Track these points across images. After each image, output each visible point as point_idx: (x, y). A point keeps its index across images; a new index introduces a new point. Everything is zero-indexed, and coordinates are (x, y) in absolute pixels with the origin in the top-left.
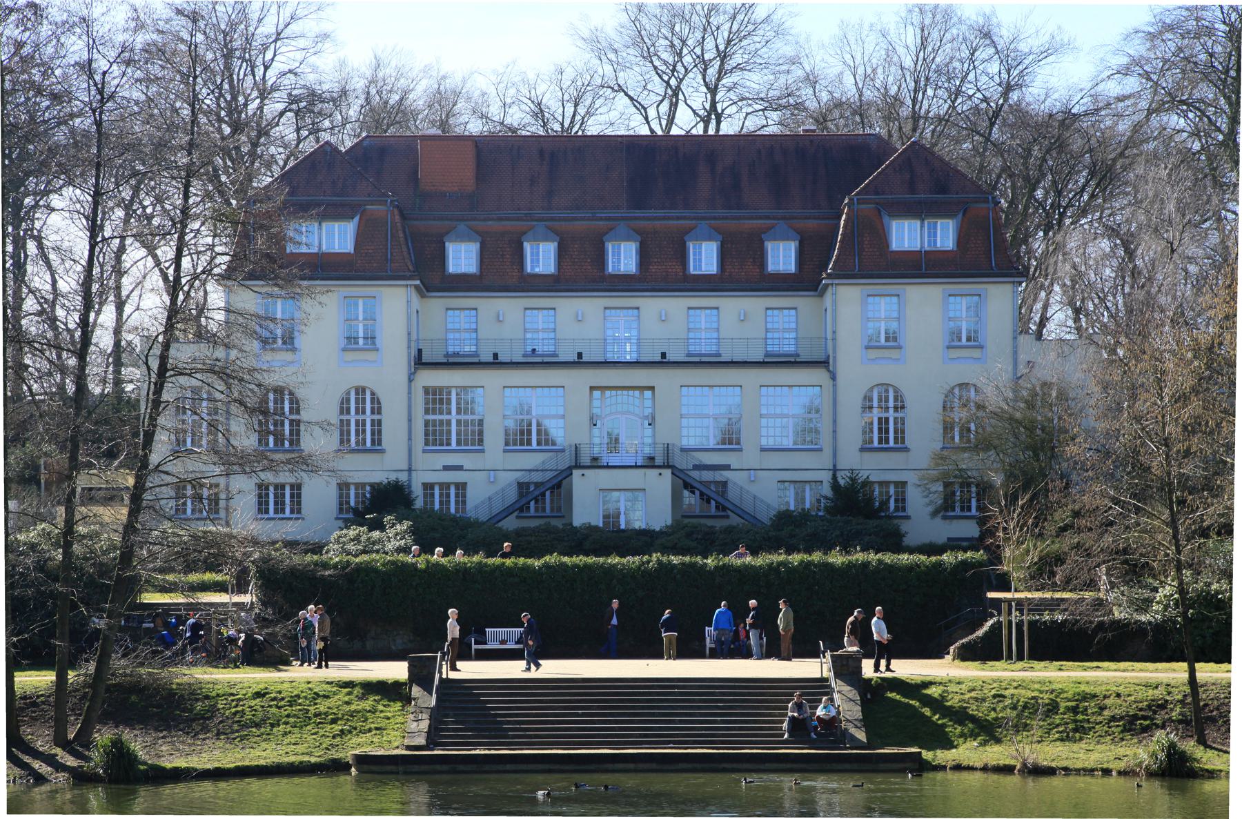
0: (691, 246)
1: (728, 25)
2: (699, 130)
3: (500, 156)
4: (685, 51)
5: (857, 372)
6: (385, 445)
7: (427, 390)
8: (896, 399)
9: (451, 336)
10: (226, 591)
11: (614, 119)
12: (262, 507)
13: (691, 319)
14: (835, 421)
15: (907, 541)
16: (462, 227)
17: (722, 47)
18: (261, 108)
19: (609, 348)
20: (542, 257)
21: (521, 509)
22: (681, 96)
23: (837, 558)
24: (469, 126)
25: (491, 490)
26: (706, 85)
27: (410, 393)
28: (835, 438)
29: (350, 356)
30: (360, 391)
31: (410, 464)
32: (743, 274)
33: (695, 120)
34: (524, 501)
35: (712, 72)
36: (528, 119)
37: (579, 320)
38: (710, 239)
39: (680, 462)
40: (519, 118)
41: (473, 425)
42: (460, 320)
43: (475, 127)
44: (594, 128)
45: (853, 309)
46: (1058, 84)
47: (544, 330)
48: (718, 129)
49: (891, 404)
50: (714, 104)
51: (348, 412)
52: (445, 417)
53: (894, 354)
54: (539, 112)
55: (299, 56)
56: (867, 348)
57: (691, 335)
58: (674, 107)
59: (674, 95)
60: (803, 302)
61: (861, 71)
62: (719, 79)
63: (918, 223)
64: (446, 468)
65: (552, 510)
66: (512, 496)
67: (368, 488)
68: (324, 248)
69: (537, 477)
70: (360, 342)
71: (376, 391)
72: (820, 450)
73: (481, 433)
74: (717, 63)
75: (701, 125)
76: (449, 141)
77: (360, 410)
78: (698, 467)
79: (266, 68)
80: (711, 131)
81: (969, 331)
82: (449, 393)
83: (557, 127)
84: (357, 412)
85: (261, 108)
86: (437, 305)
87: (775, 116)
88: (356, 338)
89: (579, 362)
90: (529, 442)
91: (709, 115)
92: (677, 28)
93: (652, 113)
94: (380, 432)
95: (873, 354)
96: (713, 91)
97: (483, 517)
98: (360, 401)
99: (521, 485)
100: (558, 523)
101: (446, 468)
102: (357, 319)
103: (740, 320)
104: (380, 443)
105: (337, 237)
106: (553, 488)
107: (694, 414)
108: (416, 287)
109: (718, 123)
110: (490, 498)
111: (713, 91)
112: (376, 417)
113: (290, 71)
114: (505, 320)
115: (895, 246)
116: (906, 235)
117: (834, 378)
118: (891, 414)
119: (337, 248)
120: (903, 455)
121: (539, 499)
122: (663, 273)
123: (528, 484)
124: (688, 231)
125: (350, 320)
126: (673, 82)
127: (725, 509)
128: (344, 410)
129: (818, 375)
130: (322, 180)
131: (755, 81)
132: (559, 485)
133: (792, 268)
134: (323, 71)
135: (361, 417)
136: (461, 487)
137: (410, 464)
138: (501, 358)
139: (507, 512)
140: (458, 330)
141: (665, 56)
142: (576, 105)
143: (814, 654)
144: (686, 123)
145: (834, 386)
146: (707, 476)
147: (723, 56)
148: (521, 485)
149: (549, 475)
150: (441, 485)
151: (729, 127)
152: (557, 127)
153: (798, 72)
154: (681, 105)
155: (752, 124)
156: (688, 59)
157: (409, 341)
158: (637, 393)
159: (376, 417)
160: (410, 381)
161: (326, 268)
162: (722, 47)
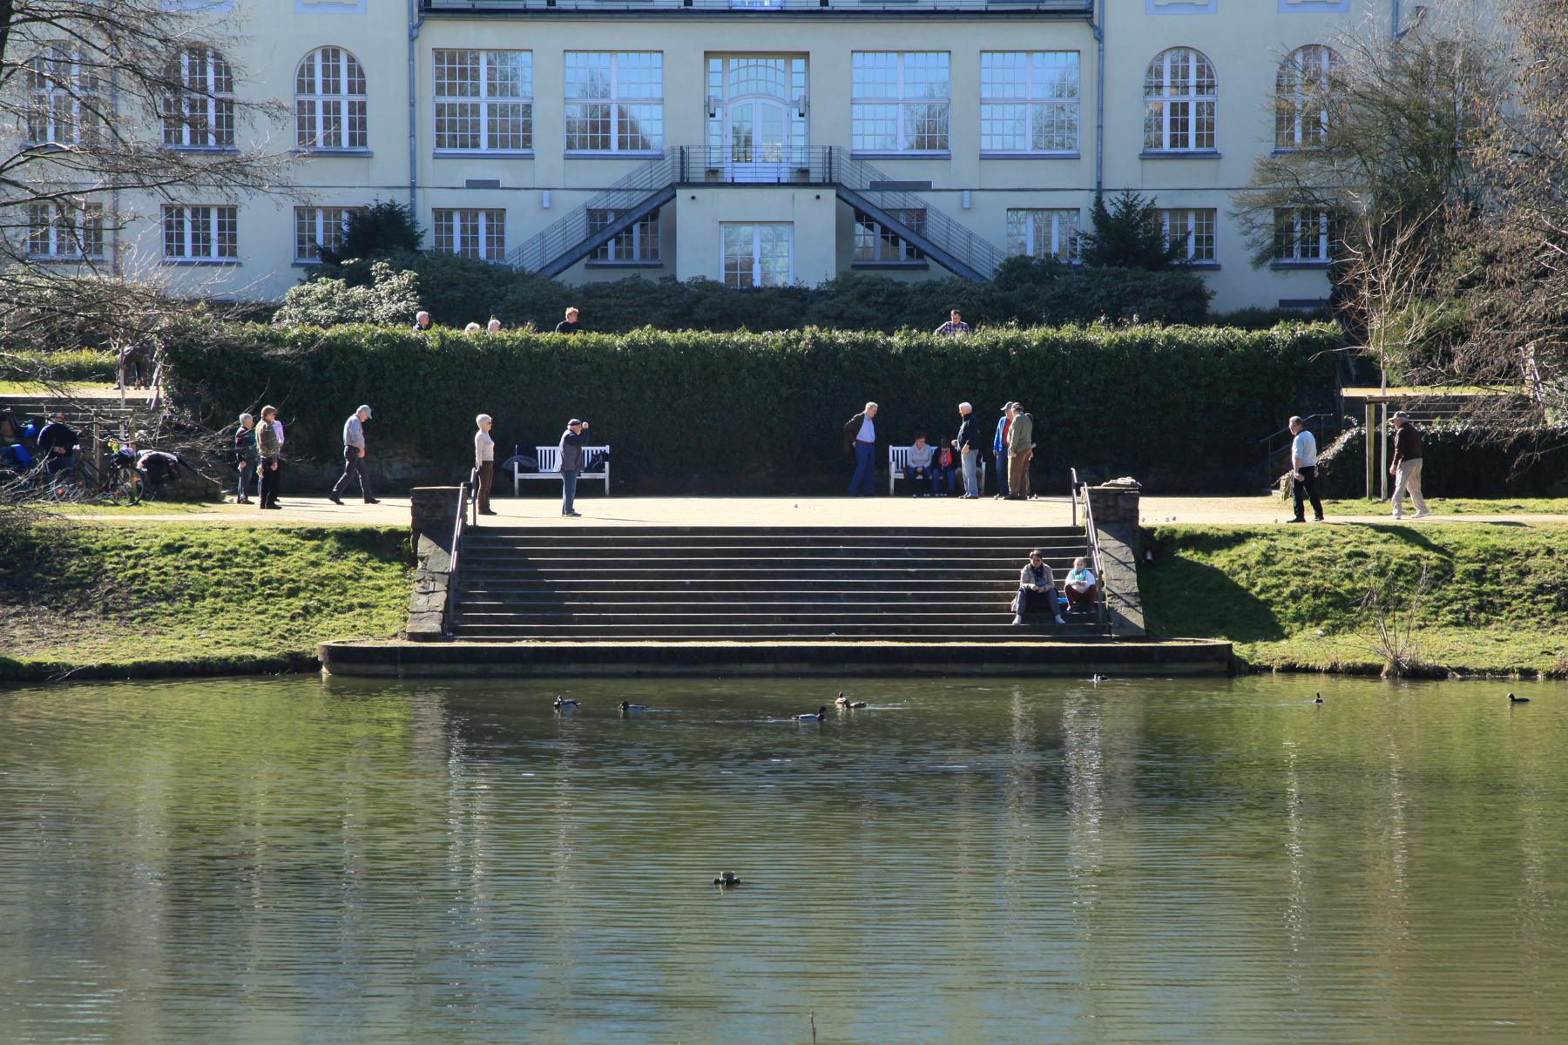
6: (372, 144)
7: (439, 55)
12: (173, 242)
14: (1101, 110)
15: (1214, 306)
21: (593, 254)
27: (411, 58)
30: (330, 53)
31: (413, 177)
34: (597, 240)
39: (851, 177)
41: (452, 113)
49: (1193, 80)
52: (473, 100)
64: (472, 184)
65: (643, 255)
66: (578, 232)
69: (619, 201)
72: (1077, 157)
73: (528, 127)
77: (331, 87)
78: (877, 186)
82: (476, 60)
90: (476, 145)
97: (532, 266)
98: (331, 71)
100: (652, 277)
101: (472, 184)
104: (363, 142)
106: (644, 219)
110: (542, 235)
112: (357, 98)
117: (1100, 38)
118: (1192, 98)
123: (603, 213)
132: (654, 214)
136: (496, 216)
137: (413, 177)
139: (570, 258)
143: (1062, 488)
146: (893, 200)
150: (464, 212)
158: (781, 62)
159: (357, 98)
160: (412, 38)
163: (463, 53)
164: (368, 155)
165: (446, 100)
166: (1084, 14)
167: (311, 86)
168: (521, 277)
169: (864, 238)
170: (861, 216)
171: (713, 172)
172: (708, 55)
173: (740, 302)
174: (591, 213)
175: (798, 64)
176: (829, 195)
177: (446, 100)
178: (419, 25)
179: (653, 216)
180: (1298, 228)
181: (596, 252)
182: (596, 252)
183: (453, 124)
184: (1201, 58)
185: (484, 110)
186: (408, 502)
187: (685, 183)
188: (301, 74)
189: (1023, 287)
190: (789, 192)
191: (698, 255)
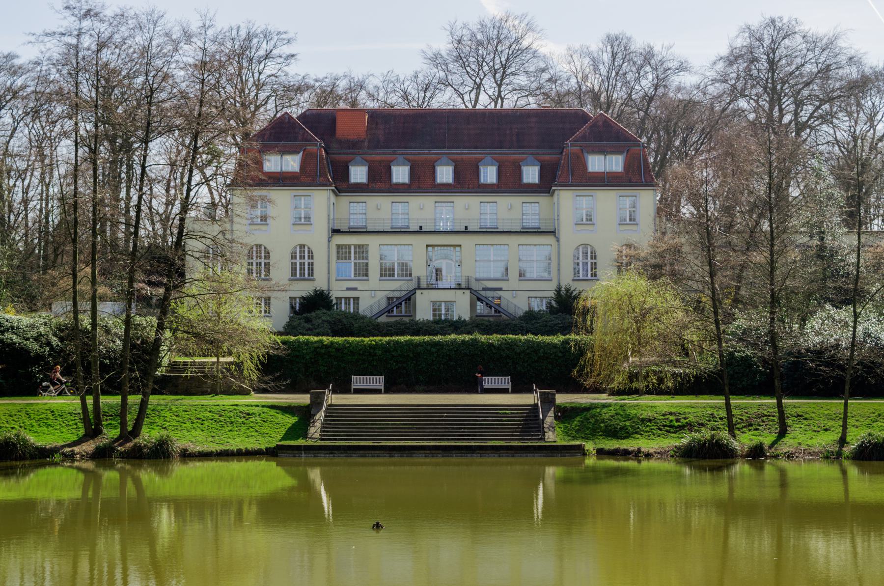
0: (482, 168)
1: (507, 51)
2: (492, 106)
3: (382, 119)
4: (484, 64)
5: (571, 237)
6: (315, 276)
7: (338, 246)
8: (592, 253)
9: (352, 217)
11: (444, 100)
13: (438, 210)
14: (559, 264)
16: (358, 158)
17: (504, 63)
18: (257, 95)
19: (437, 224)
20: (401, 174)
21: (389, 312)
22: (482, 88)
23: (402, 339)
24: (368, 103)
25: (372, 302)
26: (496, 82)
27: (329, 248)
30: (302, 246)
32: (509, 183)
33: (489, 101)
34: (390, 307)
35: (498, 76)
36: (400, 100)
37: (421, 209)
38: (492, 165)
39: (475, 286)
40: (395, 100)
42: (357, 208)
43: (371, 105)
44: (435, 104)
45: (569, 202)
46: (685, 82)
47: (402, 214)
48: (502, 105)
49: (263, 255)
50: (500, 92)
52: (357, 261)
53: (591, 228)
54: (406, 96)
55: (278, 66)
56: (576, 224)
57: (394, 217)
58: (478, 95)
59: (478, 87)
60: (543, 200)
61: (580, 75)
62: (502, 80)
63: (603, 157)
64: (348, 289)
65: (406, 312)
66: (384, 304)
67: (298, 300)
68: (284, 169)
69: (397, 294)
71: (268, 248)
72: (551, 280)
73: (367, 270)
74: (501, 70)
75: (493, 104)
76: (355, 110)
78: (484, 289)
79: (260, 73)
80: (499, 107)
81: (587, 215)
82: (350, 248)
83: (415, 104)
85: (257, 95)
86: (345, 200)
87: (531, 99)
89: (420, 232)
90: (393, 275)
91: (497, 99)
92: (480, 52)
93: (466, 97)
94: (312, 270)
95: (579, 228)
96: (500, 86)
97: (369, 314)
98: (258, 252)
99: (389, 299)
100: (407, 320)
101: (348, 289)
103: (508, 209)
104: (312, 275)
105: (292, 163)
106: (406, 300)
107: (484, 262)
108: (333, 190)
109: (502, 102)
110: (371, 306)
111: (500, 86)
112: (311, 261)
113: (273, 75)
114: (379, 209)
115: (591, 169)
116: (596, 163)
117: (558, 241)
118: (263, 261)
119: (290, 169)
121: (399, 306)
122: (466, 182)
123: (392, 298)
124: (480, 160)
126: (478, 80)
127: (499, 312)
128: (293, 256)
129: (550, 239)
130: (282, 133)
131: (522, 80)
132: (409, 299)
133: (536, 181)
134: (295, 72)
135: (302, 261)
136: (356, 299)
138: (470, 229)
139: (381, 313)
140: (356, 214)
141: (473, 67)
142: (425, 92)
143: (530, 391)
144: (484, 102)
146: (489, 294)
147: (504, 67)
148: (389, 299)
149: (403, 293)
150: (346, 298)
151: (508, 104)
152: (415, 104)
153: (546, 76)
154: (482, 92)
155: (522, 103)
156: (486, 68)
157: (329, 219)
158: (452, 248)
159: (311, 261)
160: (329, 241)
161: (281, 180)
162: (504, 63)
163: (363, 246)
166: (553, 233)
168: (364, 317)
169: (480, 308)
170: (479, 299)
171: (459, 284)
172: (428, 246)
173: (441, 325)
174: (389, 299)
175: (458, 249)
176: (468, 292)
177: (365, 261)
179: (409, 299)
180: (14, 337)
181: (390, 311)
182: (390, 311)
183: (359, 269)
185: (581, 264)
186: (309, 396)
187: (419, 288)
189: (530, 321)
190: (453, 291)
191: (423, 312)
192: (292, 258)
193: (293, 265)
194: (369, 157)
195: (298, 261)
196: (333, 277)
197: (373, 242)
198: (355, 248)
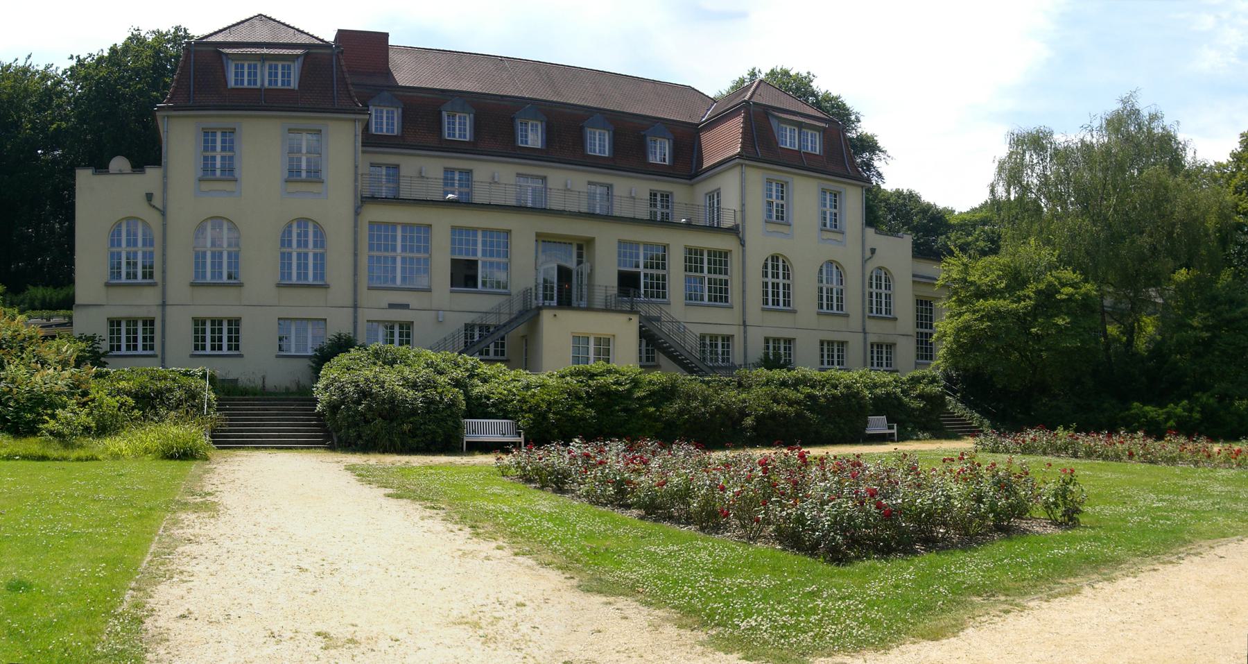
7: (726, 254)
10: (893, 441)
12: (199, 344)
14: (744, 283)
15: (305, 381)
27: (356, 226)
28: (744, 297)
29: (292, 187)
30: (303, 222)
31: (355, 300)
41: (658, 279)
51: (290, 245)
52: (408, 255)
64: (392, 306)
70: (301, 175)
77: (303, 243)
82: (702, 254)
84: (299, 245)
88: (299, 172)
101: (392, 306)
102: (300, 151)
117: (743, 245)
118: (781, 281)
120: (321, 292)
125: (294, 150)
128: (285, 241)
137: (355, 300)
145: (744, 251)
159: (286, 250)
164: (240, 285)
165: (723, 277)
167: (290, 242)
178: (361, 207)
184: (317, 226)
188: (283, 235)
192: (283, 245)
193: (115, 256)
194: (644, 309)
195: (124, 250)
196: (364, 282)
197: (360, 172)
198: (709, 255)
